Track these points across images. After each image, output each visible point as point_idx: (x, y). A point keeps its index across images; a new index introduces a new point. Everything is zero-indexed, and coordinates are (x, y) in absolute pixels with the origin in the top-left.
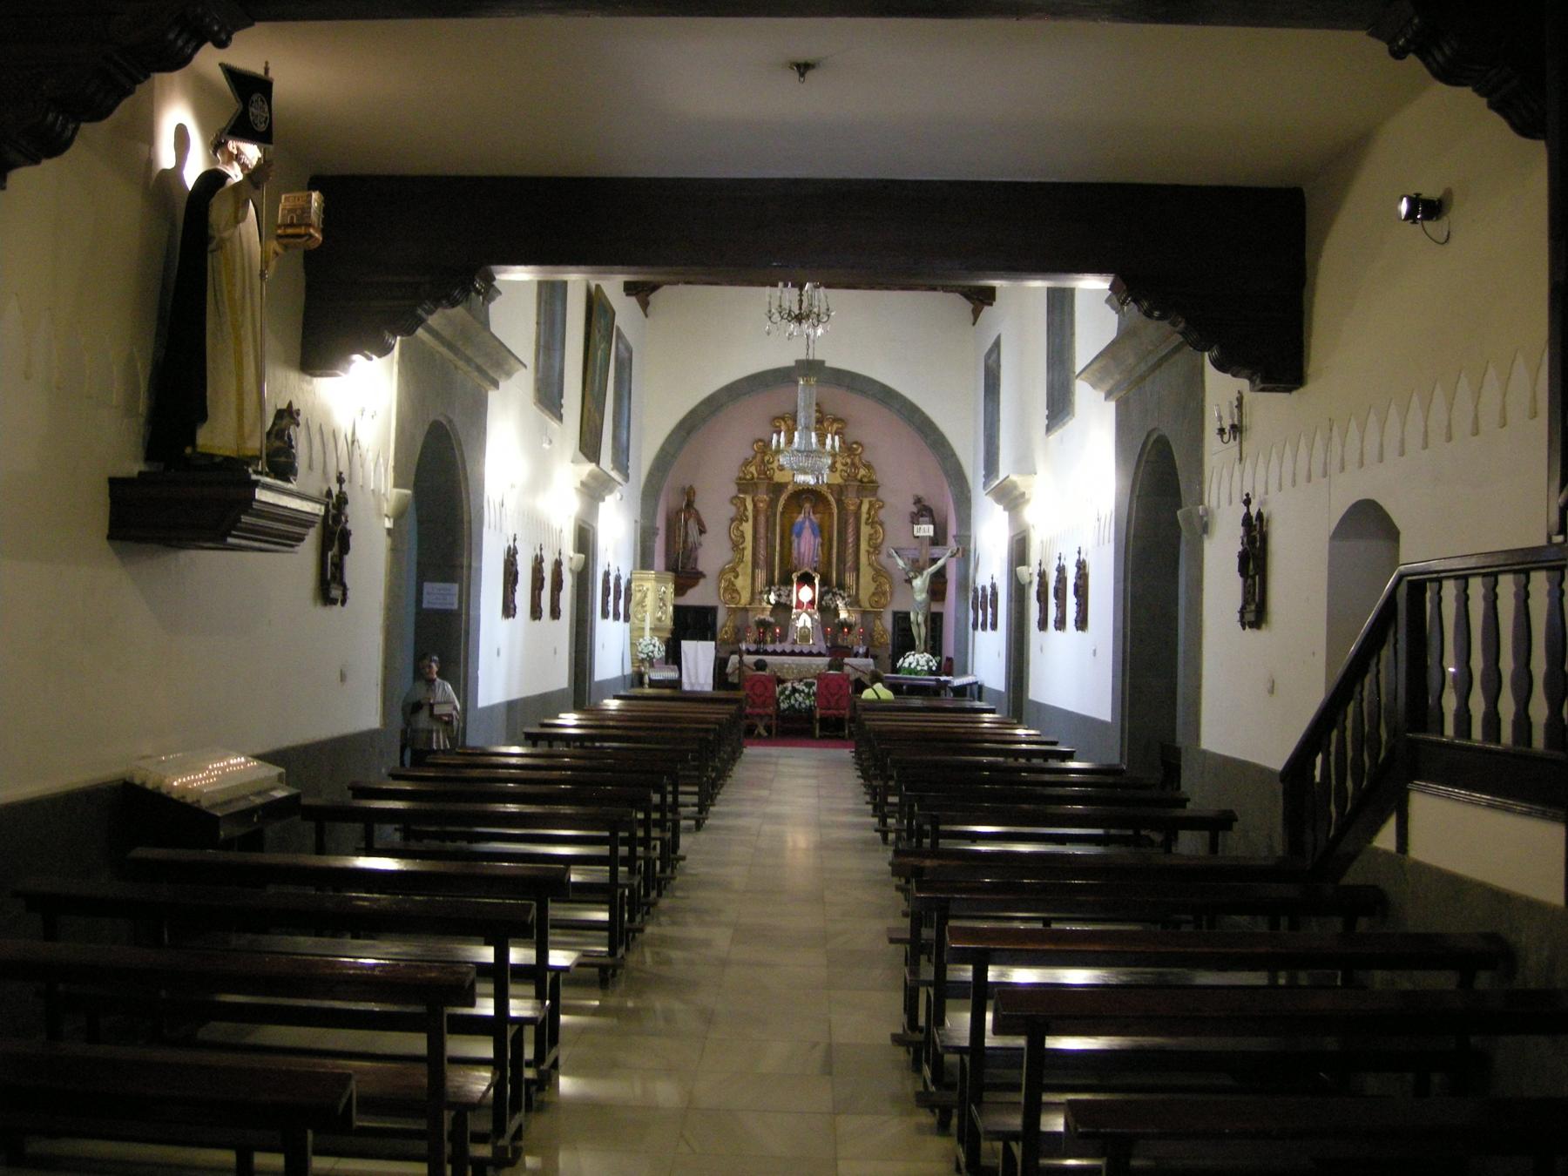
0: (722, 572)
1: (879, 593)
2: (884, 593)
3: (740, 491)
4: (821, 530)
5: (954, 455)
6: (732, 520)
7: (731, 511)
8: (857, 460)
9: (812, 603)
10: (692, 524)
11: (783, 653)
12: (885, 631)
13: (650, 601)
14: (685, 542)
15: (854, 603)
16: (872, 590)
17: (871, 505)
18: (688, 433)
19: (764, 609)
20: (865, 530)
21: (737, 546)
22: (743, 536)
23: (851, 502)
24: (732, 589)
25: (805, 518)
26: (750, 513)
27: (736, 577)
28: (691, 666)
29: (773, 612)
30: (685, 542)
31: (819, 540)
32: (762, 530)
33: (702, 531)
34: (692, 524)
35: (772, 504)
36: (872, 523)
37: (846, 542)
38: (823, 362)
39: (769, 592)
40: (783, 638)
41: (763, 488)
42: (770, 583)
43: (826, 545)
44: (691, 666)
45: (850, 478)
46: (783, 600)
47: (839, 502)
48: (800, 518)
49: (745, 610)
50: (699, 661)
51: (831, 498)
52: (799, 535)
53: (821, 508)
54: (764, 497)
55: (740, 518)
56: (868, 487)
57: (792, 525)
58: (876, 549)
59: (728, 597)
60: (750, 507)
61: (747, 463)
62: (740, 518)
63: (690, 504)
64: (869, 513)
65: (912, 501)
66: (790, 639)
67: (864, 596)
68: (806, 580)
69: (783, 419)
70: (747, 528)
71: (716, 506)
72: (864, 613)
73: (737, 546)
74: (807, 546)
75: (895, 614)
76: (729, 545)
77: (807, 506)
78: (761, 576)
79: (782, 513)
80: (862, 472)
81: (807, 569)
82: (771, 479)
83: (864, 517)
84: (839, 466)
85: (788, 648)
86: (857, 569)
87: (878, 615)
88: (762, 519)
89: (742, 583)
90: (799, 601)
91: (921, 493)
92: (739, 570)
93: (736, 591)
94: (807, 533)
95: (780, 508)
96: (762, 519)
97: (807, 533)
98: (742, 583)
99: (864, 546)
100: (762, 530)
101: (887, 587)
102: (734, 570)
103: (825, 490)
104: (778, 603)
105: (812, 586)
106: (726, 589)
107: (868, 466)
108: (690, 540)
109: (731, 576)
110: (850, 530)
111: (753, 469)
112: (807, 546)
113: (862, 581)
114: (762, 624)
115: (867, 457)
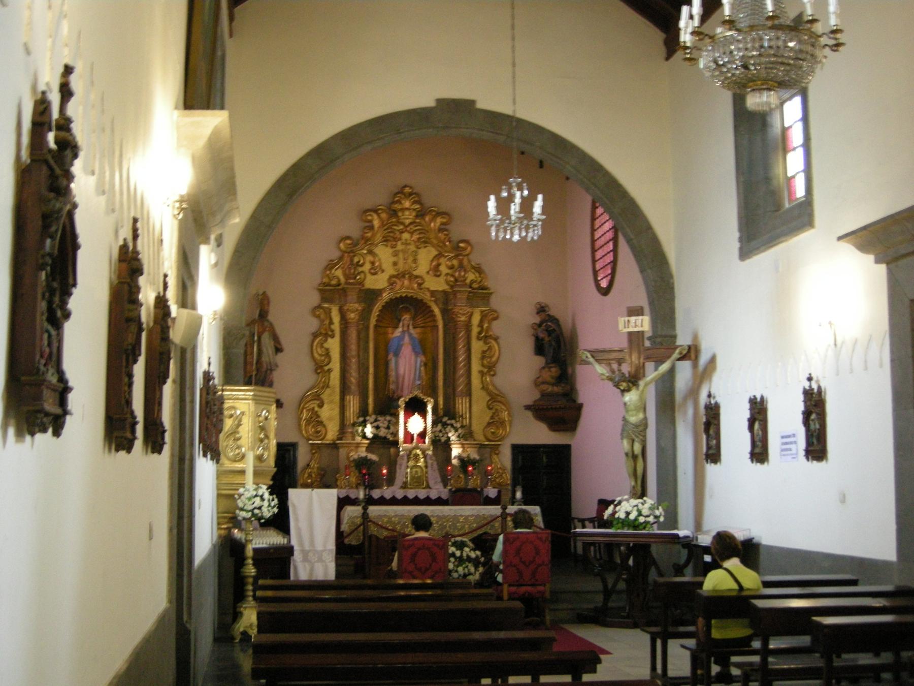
0: (303, 400)
1: (495, 422)
2: (502, 423)
3: (324, 299)
4: (423, 347)
5: (649, 228)
6: (315, 335)
7: (313, 324)
8: (465, 262)
9: (422, 435)
10: (266, 339)
11: (394, 501)
12: (504, 469)
13: (246, 430)
14: (259, 362)
15: (467, 436)
16: (487, 419)
17: (484, 317)
18: (290, 196)
19: (358, 445)
20: (477, 346)
21: (320, 368)
22: (327, 354)
23: (461, 311)
24: (316, 421)
25: (404, 334)
26: (336, 326)
27: (321, 406)
28: (303, 525)
29: (369, 449)
30: (259, 362)
31: (421, 358)
32: (353, 347)
33: (278, 349)
34: (266, 339)
35: (365, 315)
36: (485, 337)
37: (455, 358)
38: (473, 102)
39: (364, 424)
40: (391, 480)
41: (352, 296)
42: (364, 412)
43: (431, 366)
44: (303, 525)
45: (456, 283)
46: (383, 432)
47: (445, 312)
48: (398, 332)
49: (334, 446)
50: (315, 516)
51: (436, 311)
52: (397, 354)
53: (420, 321)
54: (354, 308)
55: (323, 333)
56: (480, 294)
57: (387, 343)
58: (490, 369)
59: (311, 430)
60: (336, 319)
61: (331, 266)
62: (323, 333)
63: (263, 315)
64: (481, 325)
65: (275, 384)
66: (399, 481)
67: (478, 427)
68: (415, 406)
69: (376, 211)
70: (334, 345)
71: (294, 319)
72: (481, 447)
73: (320, 368)
74: (407, 366)
75: (517, 449)
76: (309, 365)
77: (406, 317)
78: (353, 404)
79: (376, 326)
80: (471, 276)
81: (417, 393)
82: (361, 283)
83: (475, 330)
84: (443, 269)
85: (399, 495)
86: (469, 393)
87: (495, 449)
88: (353, 334)
89: (329, 413)
90: (407, 433)
91: (542, 299)
92: (324, 397)
93: (321, 423)
94: (407, 351)
95: (373, 321)
96: (353, 334)
97: (407, 351)
98: (329, 413)
99: (476, 367)
100: (353, 347)
101: (505, 415)
102: (317, 397)
103: (427, 297)
104: (375, 437)
105: (423, 414)
106: (308, 422)
107: (478, 270)
108: (265, 359)
109: (314, 405)
110: (461, 345)
111: (339, 273)
112: (407, 366)
113: (475, 408)
114: (361, 463)
115: (475, 258)
